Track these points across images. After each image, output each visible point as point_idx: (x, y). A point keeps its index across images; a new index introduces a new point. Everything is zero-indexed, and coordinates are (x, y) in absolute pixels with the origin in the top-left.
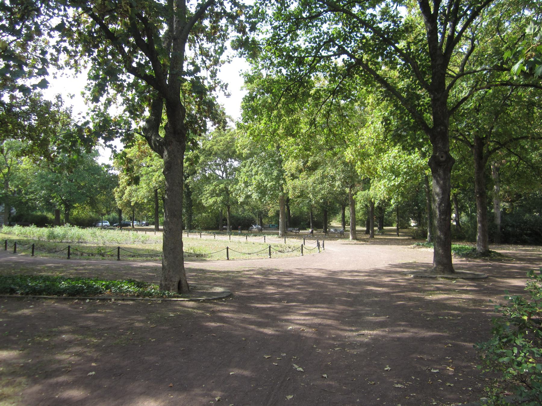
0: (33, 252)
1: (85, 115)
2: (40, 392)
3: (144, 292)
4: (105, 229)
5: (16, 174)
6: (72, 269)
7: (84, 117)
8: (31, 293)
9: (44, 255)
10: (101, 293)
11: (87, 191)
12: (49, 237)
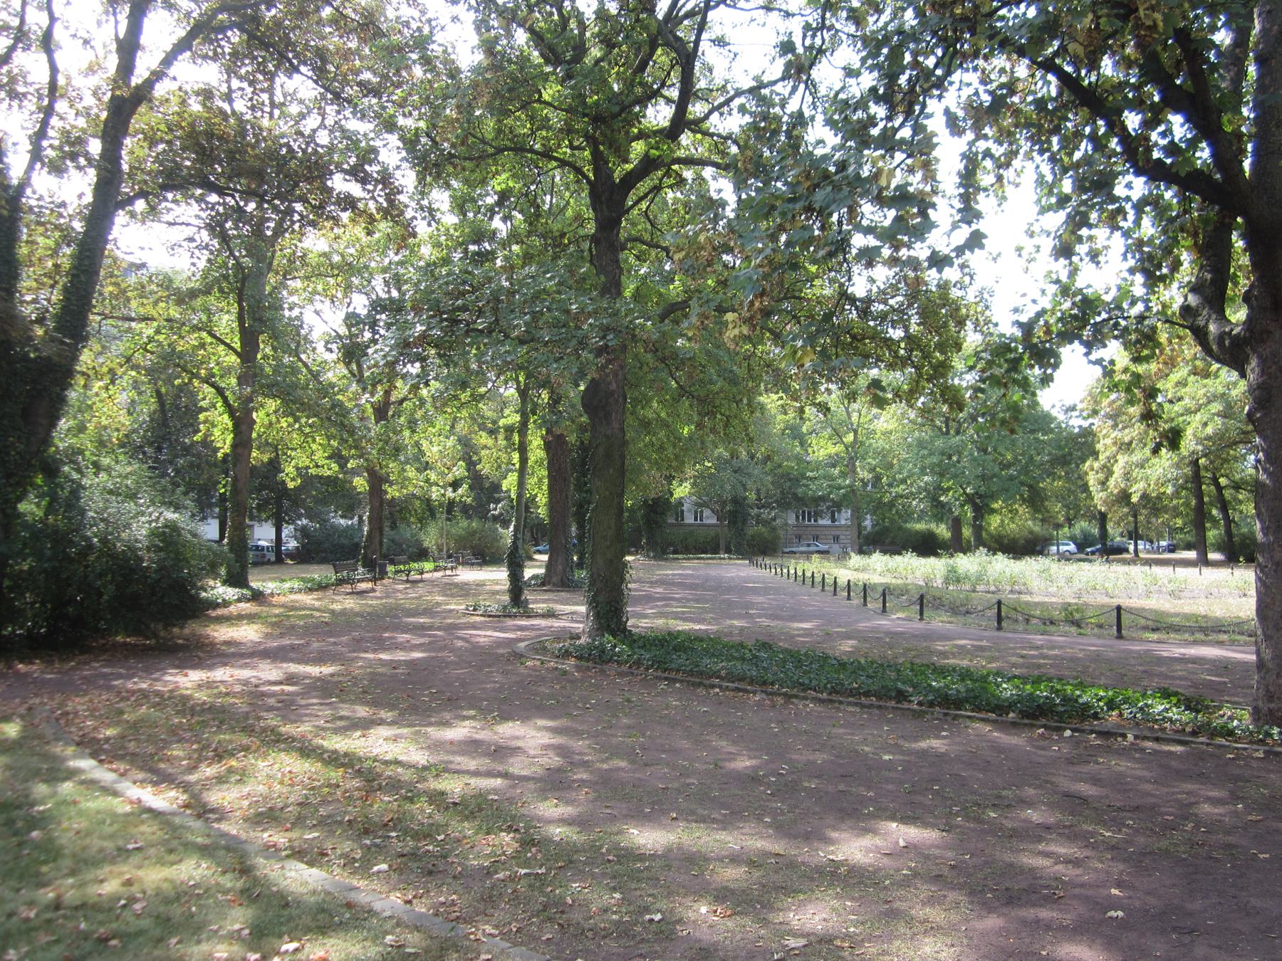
0: (921, 613)
1: (1037, 295)
2: (999, 932)
3: (1209, 724)
4: (1068, 560)
5: (870, 445)
6: (1013, 655)
7: (1034, 301)
8: (940, 705)
9: (945, 619)
10: (1096, 716)
11: (1019, 472)
12: (947, 580)
